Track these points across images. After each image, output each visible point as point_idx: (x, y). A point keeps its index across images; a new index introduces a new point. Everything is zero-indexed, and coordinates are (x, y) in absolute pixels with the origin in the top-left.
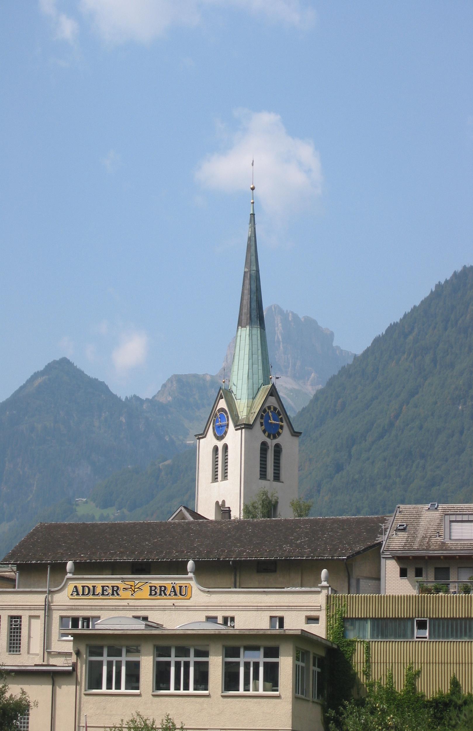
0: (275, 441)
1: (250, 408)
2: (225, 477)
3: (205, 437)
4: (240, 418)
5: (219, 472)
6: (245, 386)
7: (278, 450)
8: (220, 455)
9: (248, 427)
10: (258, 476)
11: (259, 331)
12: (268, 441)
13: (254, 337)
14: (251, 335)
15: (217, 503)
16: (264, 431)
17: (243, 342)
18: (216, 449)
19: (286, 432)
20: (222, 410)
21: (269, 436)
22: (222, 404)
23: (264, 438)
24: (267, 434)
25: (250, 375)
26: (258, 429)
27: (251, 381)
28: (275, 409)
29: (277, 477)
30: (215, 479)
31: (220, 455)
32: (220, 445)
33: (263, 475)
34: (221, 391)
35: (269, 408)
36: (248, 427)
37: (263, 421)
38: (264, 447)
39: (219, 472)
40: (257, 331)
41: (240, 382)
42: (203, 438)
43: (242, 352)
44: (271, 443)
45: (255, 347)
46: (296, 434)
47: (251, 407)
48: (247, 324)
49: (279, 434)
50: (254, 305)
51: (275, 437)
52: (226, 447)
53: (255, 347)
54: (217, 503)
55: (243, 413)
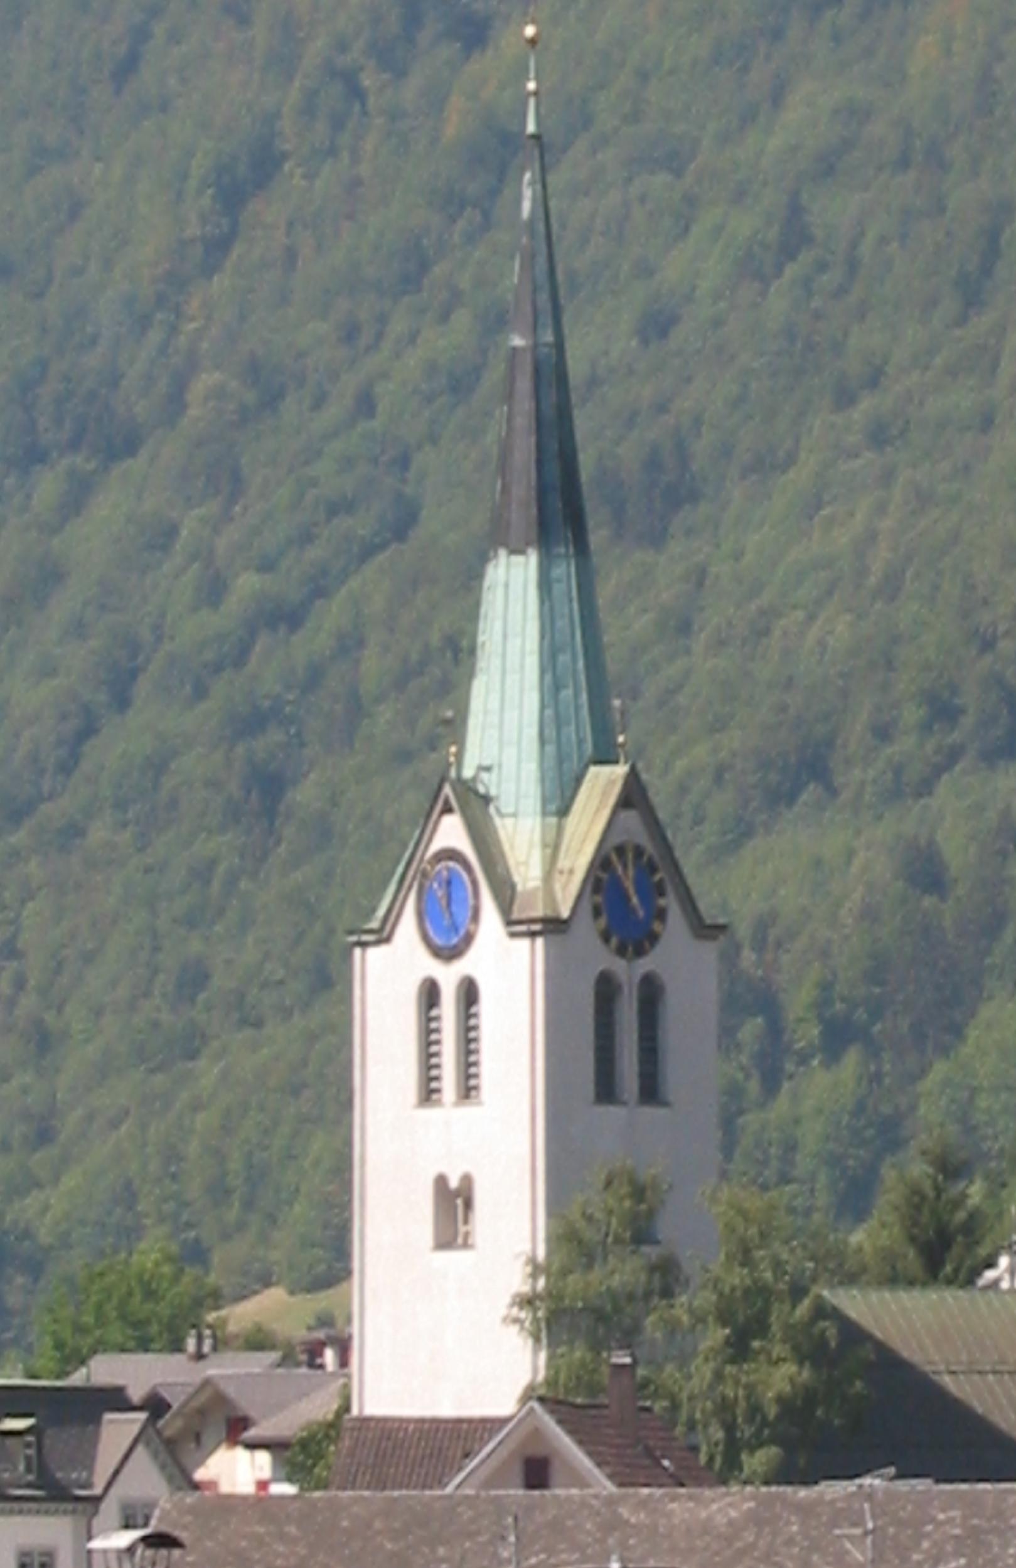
0: (645, 965)
1: (553, 848)
2: (468, 1090)
3: (387, 940)
4: (519, 888)
5: (448, 1063)
6: (531, 768)
7: (651, 993)
8: (448, 1025)
9: (552, 927)
10: (590, 1089)
11: (573, 569)
12: (618, 966)
13: (558, 589)
14: (545, 584)
15: (441, 1181)
16: (606, 937)
17: (516, 609)
18: (430, 993)
19: (675, 928)
20: (451, 854)
21: (621, 951)
22: (451, 832)
23: (606, 960)
24: (614, 941)
25: (551, 732)
26: (587, 930)
27: (550, 749)
28: (639, 852)
29: (651, 1091)
30: (428, 1094)
31: (448, 1025)
32: (448, 977)
33: (606, 1090)
34: (447, 790)
35: (620, 850)
36: (552, 927)
37: (599, 899)
38: (606, 990)
39: (448, 1063)
40: (565, 570)
41: (511, 753)
42: (378, 942)
43: (514, 644)
44: (628, 973)
45: (562, 623)
46: (705, 930)
47: (556, 847)
48: (528, 544)
49: (654, 938)
50: (554, 470)
51: (640, 952)
52: (469, 993)
53: (562, 623)
54: (441, 1181)
55: (526, 867)
